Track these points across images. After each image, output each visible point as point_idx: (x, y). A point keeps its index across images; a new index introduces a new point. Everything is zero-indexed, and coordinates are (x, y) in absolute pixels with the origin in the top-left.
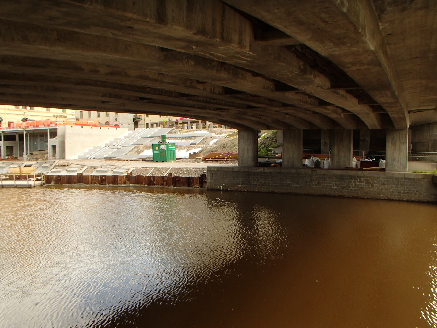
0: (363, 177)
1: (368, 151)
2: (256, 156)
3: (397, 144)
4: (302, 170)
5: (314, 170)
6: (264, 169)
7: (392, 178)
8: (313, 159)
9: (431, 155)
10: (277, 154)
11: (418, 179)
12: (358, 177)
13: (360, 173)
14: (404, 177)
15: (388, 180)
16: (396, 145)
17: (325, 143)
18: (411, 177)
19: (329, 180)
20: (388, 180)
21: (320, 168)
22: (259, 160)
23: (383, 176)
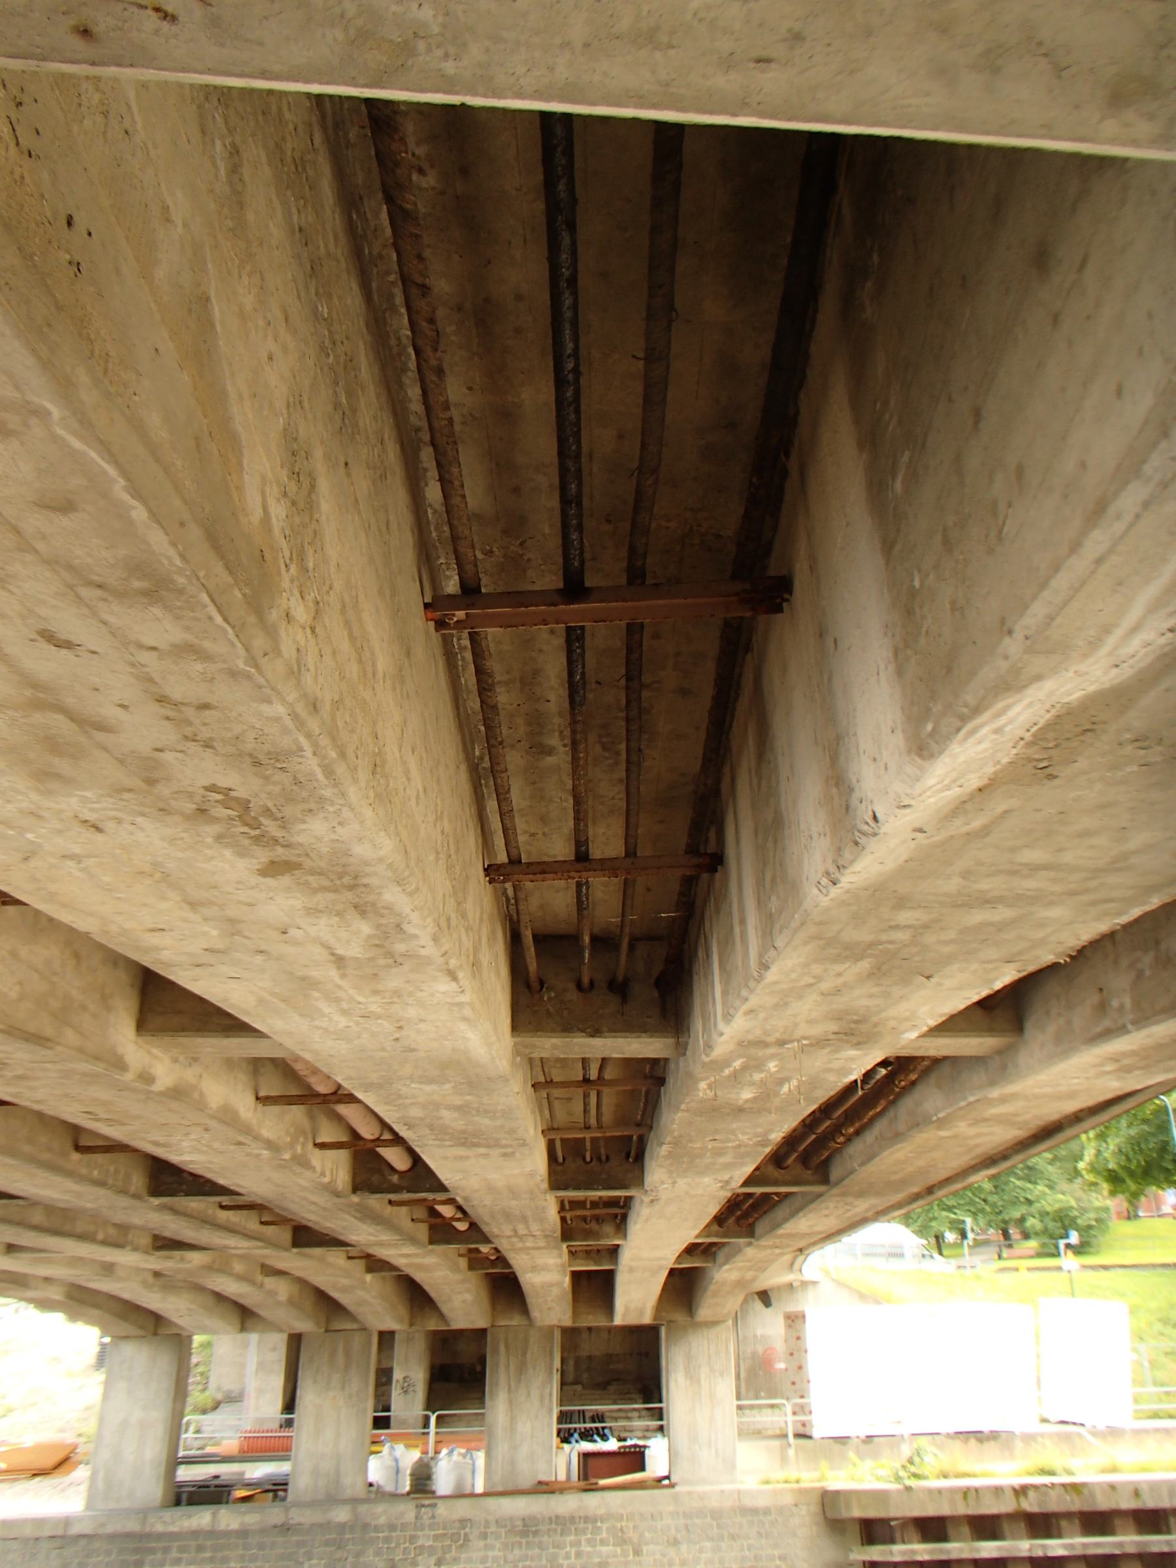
5: (423, 1506)
6: (214, 1515)
11: (781, 1510)
12: (586, 1519)
13: (592, 1501)
15: (689, 1522)
16: (699, 1382)
17: (406, 1385)
18: (761, 1503)
19: (482, 1543)
20: (689, 1522)
22: (185, 1474)
23: (671, 1508)
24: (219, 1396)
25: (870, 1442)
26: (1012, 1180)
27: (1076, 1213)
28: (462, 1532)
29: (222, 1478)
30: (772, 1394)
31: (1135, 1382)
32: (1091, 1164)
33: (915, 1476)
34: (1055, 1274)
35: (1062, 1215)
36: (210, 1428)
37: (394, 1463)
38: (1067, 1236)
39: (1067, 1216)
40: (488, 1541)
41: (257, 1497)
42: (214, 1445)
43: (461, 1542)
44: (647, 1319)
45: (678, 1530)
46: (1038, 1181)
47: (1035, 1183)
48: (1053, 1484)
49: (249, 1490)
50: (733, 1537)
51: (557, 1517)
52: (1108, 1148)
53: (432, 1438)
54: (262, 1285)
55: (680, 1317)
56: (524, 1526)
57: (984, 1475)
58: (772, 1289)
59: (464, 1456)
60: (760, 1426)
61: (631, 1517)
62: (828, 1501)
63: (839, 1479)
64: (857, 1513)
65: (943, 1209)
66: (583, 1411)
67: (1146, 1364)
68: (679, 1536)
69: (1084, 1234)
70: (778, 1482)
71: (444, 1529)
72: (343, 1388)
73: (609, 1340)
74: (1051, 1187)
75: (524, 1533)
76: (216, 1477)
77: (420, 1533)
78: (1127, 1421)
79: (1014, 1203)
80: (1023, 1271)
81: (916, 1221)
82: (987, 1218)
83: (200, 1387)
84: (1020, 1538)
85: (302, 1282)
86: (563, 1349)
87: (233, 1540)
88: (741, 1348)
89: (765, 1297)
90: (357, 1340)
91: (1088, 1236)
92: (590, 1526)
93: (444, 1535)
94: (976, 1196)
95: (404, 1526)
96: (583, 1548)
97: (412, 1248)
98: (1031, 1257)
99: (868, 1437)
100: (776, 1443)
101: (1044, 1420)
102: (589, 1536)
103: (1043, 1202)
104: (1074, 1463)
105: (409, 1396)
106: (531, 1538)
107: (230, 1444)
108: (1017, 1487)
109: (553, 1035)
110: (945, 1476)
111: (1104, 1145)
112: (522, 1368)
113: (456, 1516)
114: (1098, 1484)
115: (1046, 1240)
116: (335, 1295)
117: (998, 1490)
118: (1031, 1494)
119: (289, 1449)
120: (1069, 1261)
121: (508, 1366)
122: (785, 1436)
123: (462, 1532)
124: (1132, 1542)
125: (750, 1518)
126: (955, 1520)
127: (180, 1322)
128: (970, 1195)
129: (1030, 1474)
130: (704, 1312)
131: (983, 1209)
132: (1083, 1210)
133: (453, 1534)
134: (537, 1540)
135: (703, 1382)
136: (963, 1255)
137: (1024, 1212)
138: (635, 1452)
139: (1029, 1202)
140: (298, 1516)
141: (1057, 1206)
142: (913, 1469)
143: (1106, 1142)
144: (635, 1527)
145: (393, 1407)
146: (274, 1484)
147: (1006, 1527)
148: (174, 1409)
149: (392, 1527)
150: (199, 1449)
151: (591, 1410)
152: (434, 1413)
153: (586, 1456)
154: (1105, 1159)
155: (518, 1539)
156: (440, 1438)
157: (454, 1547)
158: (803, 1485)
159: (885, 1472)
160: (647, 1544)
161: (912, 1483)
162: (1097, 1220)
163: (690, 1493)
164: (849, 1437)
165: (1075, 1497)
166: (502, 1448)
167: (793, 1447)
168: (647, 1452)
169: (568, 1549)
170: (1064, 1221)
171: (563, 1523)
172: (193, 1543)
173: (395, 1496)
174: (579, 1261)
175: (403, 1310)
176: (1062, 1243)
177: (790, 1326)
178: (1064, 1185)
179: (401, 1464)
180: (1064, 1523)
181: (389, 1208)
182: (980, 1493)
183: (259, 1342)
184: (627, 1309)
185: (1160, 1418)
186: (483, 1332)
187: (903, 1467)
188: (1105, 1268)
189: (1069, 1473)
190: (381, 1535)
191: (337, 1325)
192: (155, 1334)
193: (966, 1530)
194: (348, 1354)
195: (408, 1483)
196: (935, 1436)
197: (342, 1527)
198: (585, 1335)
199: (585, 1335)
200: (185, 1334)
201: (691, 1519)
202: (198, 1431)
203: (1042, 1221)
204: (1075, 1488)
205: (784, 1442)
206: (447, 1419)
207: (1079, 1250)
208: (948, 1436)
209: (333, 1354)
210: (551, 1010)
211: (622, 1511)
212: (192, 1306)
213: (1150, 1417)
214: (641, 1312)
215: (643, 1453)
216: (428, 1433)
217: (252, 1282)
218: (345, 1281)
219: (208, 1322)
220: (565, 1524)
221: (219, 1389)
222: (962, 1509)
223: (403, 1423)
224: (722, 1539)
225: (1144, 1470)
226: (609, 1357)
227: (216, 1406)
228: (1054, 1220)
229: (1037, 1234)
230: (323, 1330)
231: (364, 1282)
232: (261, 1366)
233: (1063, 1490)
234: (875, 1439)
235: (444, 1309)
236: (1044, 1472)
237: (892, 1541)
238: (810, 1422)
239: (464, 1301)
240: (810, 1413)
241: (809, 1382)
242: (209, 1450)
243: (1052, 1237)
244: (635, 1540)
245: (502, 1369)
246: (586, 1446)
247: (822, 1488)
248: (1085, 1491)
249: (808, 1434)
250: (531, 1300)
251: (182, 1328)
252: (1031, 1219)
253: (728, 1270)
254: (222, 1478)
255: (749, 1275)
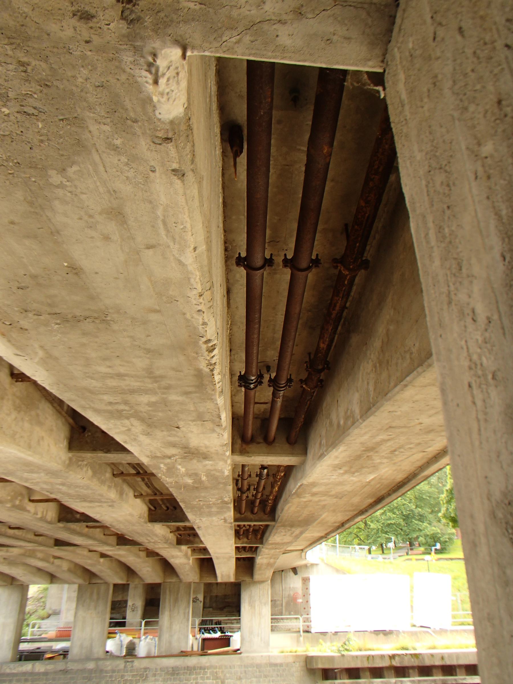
0: (208, 668)
1: (201, 619)
2: (19, 639)
3: (256, 605)
4: (108, 663)
5: (128, 662)
6: (33, 665)
7: (252, 665)
8: (122, 638)
9: (285, 621)
10: (46, 632)
11: (287, 665)
12: (201, 668)
13: (204, 660)
14: (268, 662)
15: (246, 669)
16: (255, 607)
17: (133, 608)
18: (279, 661)
19: (154, 678)
20: (246, 669)
21: (135, 656)
22: (24, 646)
23: (239, 663)
24: (50, 612)
25: (337, 635)
26: (413, 520)
27: (440, 536)
28: (145, 673)
29: (42, 649)
30: (296, 613)
31: (453, 609)
32: (444, 514)
33: (347, 650)
34: (422, 562)
35: (434, 536)
36: (45, 626)
37: (120, 643)
38: (435, 546)
39: (436, 536)
40: (156, 678)
41: (55, 657)
42: (46, 634)
43: (144, 678)
44: (232, 579)
45: (241, 673)
46: (425, 521)
47: (423, 522)
48: (406, 654)
49: (52, 654)
50: (266, 676)
51: (188, 667)
52: (451, 508)
53: (142, 631)
54: (53, 563)
55: (247, 579)
56: (173, 671)
57: (378, 650)
58: (298, 567)
59: (152, 639)
60: (290, 627)
61: (220, 667)
62: (308, 660)
63: (314, 651)
64: (320, 666)
65: (383, 533)
66: (212, 620)
67: (459, 601)
68: (242, 676)
69: (444, 545)
70: (287, 652)
71: (137, 672)
72: (95, 608)
73: (226, 588)
74: (430, 524)
75: (173, 674)
76: (39, 648)
77: (126, 674)
78: (449, 627)
79: (414, 531)
80: (414, 560)
81: (372, 538)
82: (402, 537)
83: (42, 608)
84: (392, 678)
85: (71, 562)
86: (205, 592)
87: (41, 677)
88: (283, 593)
89: (295, 570)
90: (103, 588)
91: (445, 545)
92: (202, 671)
93: (137, 675)
94: (397, 527)
95: (119, 671)
96: (198, 681)
97: (108, 547)
98: (421, 554)
99: (335, 632)
100: (295, 635)
101: (414, 626)
102: (202, 675)
103: (426, 530)
104: (417, 645)
105: (135, 612)
106: (175, 677)
107: (52, 633)
108: (391, 655)
109: (88, 452)
110: (360, 650)
111: (450, 506)
112: (176, 600)
113: (142, 666)
114: (426, 654)
115: (427, 547)
116: (89, 568)
117: (382, 657)
118: (397, 658)
119: (69, 636)
120: (433, 556)
121: (170, 600)
122: (299, 632)
123: (145, 673)
124: (440, 679)
125: (273, 668)
126: (363, 669)
127: (21, 579)
128: (395, 527)
129: (398, 649)
130: (257, 576)
131: (400, 533)
132: (443, 534)
133: (141, 674)
134: (178, 677)
135: (256, 607)
136: (390, 553)
137: (418, 534)
138: (225, 638)
139: (420, 530)
140: (71, 666)
141: (432, 532)
142: (346, 647)
143: (450, 504)
144: (222, 672)
145: (127, 618)
146: (65, 652)
147: (386, 673)
148: (18, 619)
149: (113, 671)
150: (39, 635)
151: (216, 619)
152: (144, 620)
153: (204, 640)
154: (450, 512)
155: (169, 677)
156: (146, 631)
157: (141, 680)
158: (298, 653)
159: (335, 648)
160: (227, 679)
161: (345, 653)
162: (449, 539)
163: (248, 657)
164: (327, 632)
165: (416, 660)
166: (166, 636)
167: (302, 637)
168: (231, 639)
169: (192, 681)
170: (435, 539)
171: (190, 670)
172: (23, 678)
173: (118, 657)
174: (196, 554)
175: (161, 574)
176: (433, 548)
177: (304, 583)
178: (435, 523)
179: (123, 643)
180: (411, 671)
181: (87, 529)
182: (375, 657)
183: (68, 588)
184: (222, 575)
185: (464, 625)
186: (159, 585)
187: (342, 646)
188: (452, 559)
189: (414, 649)
190: (109, 674)
191: (94, 581)
192: (11, 584)
193: (368, 673)
194: (98, 594)
195: (125, 651)
196: (365, 632)
197: (91, 671)
198: (215, 586)
199: (215, 586)
200: (25, 584)
201: (248, 668)
202: (39, 628)
203: (425, 539)
204: (416, 656)
205: (298, 634)
206: (151, 623)
207: (437, 552)
208: (371, 632)
209: (92, 594)
210: (89, 441)
211: (217, 664)
212: (25, 572)
213: (460, 625)
214: (229, 576)
215: (229, 639)
216: (141, 629)
217: (48, 562)
218: (89, 561)
219: (34, 579)
220: (191, 670)
221: (50, 609)
222: (366, 665)
223: (131, 625)
224: (260, 677)
225: (447, 648)
226: (225, 596)
227: (49, 616)
228: (430, 538)
229: (423, 544)
230: (88, 583)
231: (99, 562)
232: (69, 599)
233: (410, 656)
234: (339, 633)
235: (140, 573)
236: (403, 648)
237: (336, 679)
238: (310, 625)
239: (148, 571)
240: (311, 621)
241: (310, 608)
242: (43, 636)
243: (429, 546)
244: (222, 677)
245: (167, 601)
246: (207, 635)
247: (306, 655)
248: (420, 657)
249: (310, 631)
250: (178, 570)
251: (23, 582)
252: (421, 537)
253: (261, 558)
254: (42, 649)
255: (272, 561)
